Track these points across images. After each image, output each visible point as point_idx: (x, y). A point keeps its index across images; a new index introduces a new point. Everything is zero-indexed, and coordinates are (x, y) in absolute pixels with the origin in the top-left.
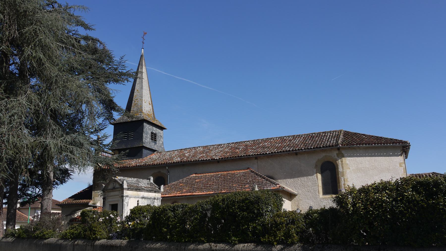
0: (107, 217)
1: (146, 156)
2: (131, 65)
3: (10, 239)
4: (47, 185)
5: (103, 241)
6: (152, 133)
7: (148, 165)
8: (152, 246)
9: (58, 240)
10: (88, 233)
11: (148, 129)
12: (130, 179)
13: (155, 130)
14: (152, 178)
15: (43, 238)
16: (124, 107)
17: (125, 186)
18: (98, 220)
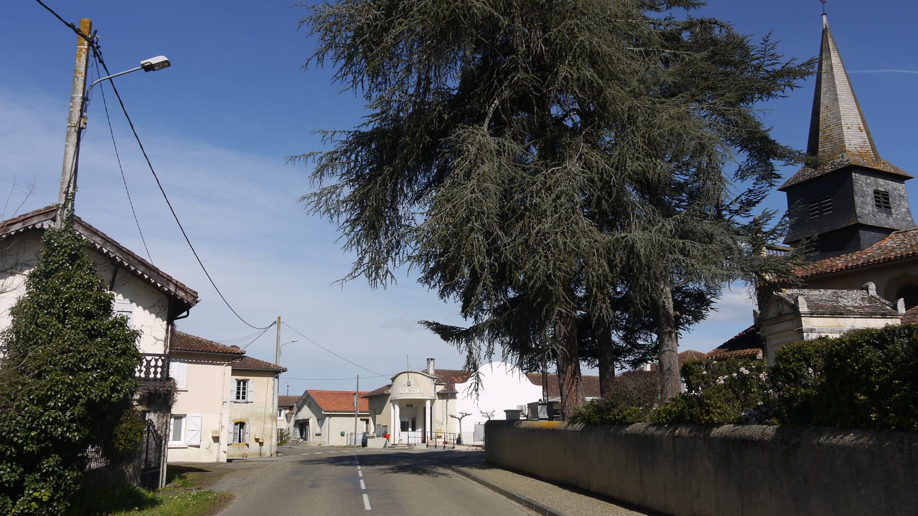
0: (735, 375)
1: (871, 245)
2: (792, 51)
3: (578, 426)
4: (668, 325)
5: (726, 429)
6: (876, 192)
7: (873, 263)
8: (834, 441)
9: (648, 427)
10: (696, 410)
11: (864, 186)
12: (817, 292)
13: (883, 184)
14: (872, 286)
15: (623, 423)
16: (800, 144)
17: (803, 308)
18: (715, 382)
